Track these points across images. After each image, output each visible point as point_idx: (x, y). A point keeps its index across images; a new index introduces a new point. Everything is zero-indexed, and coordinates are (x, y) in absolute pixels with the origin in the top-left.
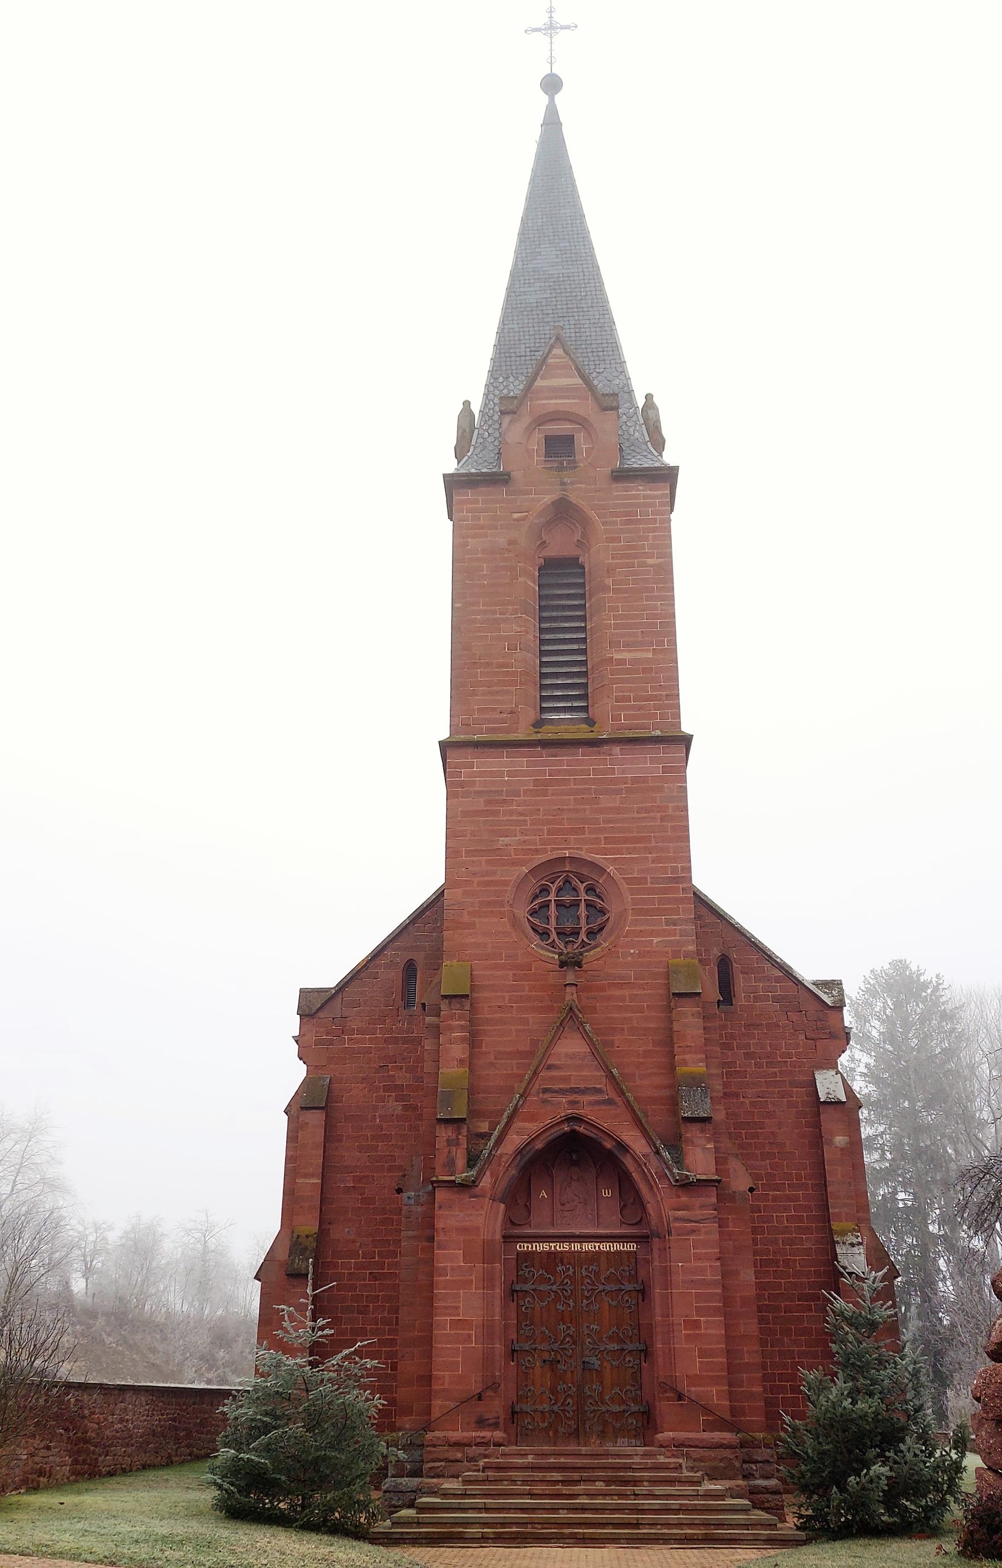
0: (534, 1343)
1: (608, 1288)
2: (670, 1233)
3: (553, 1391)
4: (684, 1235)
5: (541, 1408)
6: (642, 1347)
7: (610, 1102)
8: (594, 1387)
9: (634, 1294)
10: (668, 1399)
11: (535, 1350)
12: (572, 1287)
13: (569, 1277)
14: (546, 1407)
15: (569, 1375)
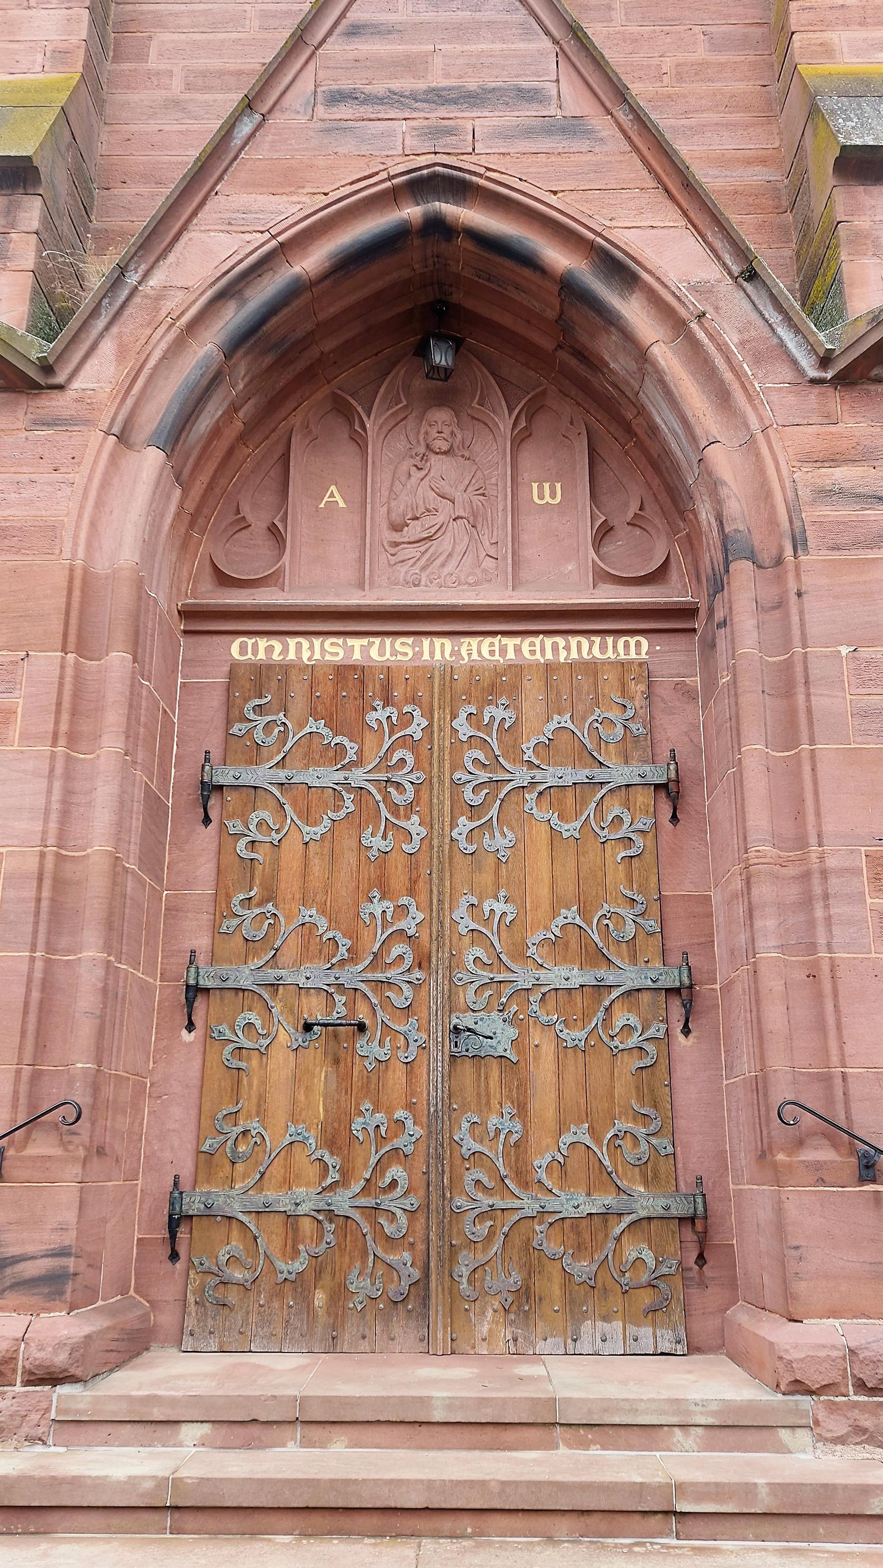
0: (273, 962)
1: (550, 776)
2: (799, 543)
3: (336, 1138)
4: (856, 544)
5: (284, 1204)
6: (671, 980)
7: (572, 127)
8: (493, 1121)
9: (643, 798)
10: (819, 1174)
11: (274, 987)
12: (418, 776)
13: (407, 742)
14: (306, 1197)
15: (397, 1076)
